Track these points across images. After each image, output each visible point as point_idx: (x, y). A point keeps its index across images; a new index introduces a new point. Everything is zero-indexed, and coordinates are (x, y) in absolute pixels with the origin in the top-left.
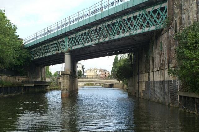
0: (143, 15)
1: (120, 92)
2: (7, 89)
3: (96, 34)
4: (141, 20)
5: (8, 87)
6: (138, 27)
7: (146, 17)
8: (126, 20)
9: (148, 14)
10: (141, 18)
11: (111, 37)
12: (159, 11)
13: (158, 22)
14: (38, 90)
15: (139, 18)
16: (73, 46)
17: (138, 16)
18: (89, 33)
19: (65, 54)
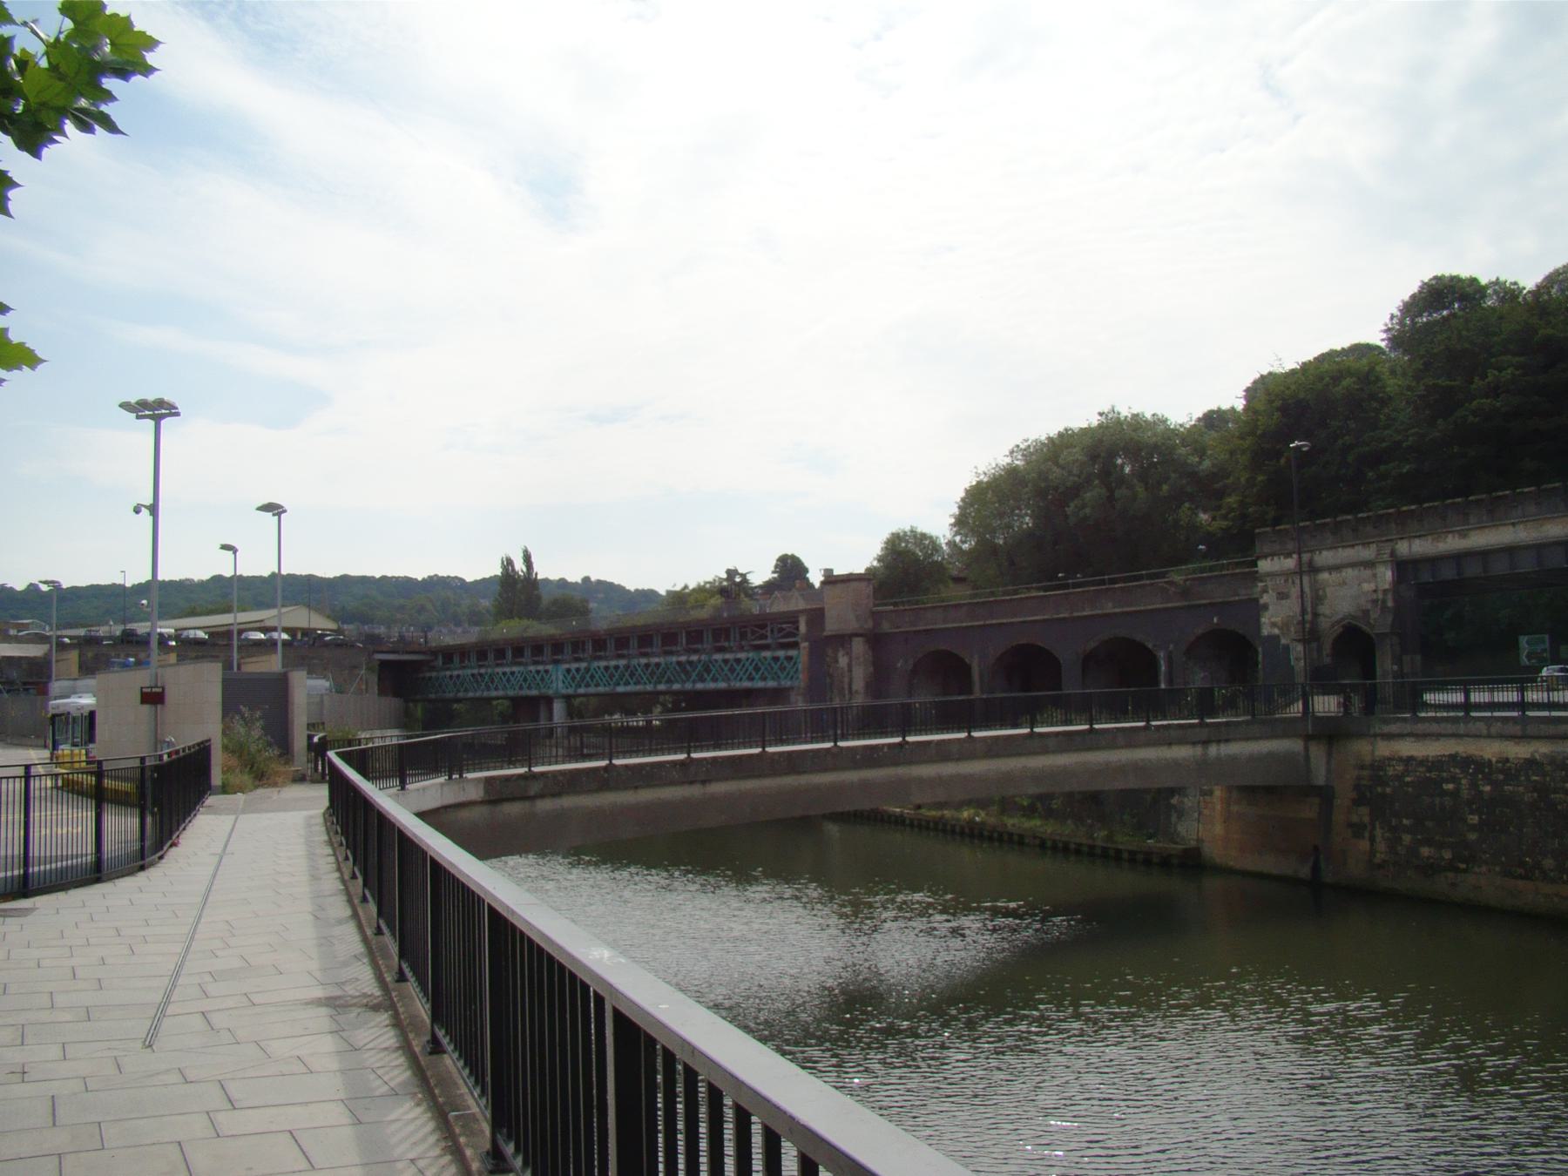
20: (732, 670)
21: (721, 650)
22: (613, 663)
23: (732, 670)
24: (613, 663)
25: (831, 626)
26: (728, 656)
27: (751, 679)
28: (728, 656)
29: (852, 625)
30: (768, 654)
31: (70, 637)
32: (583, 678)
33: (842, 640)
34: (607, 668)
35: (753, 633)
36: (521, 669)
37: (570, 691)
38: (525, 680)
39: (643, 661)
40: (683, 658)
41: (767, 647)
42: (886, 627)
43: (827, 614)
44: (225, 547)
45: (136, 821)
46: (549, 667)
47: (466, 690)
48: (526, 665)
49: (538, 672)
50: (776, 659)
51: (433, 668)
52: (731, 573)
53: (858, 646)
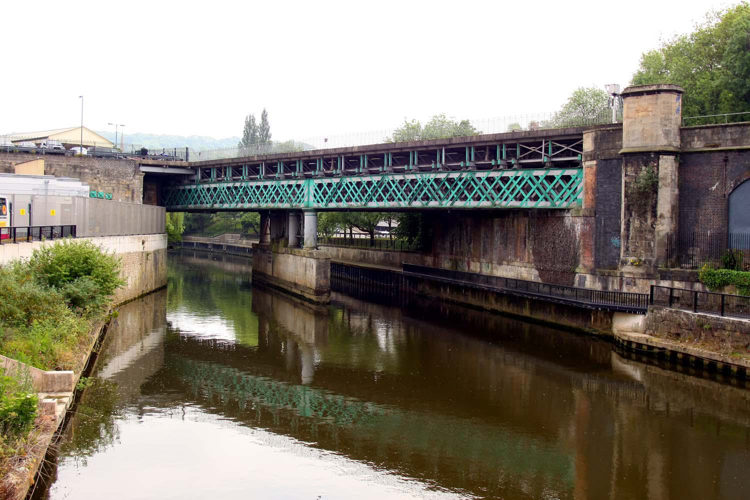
0: (275, 187)
1: (108, 253)
2: (747, 313)
3: (402, 190)
4: (273, 193)
5: (359, 269)
6: (269, 200)
7: (474, 186)
8: (261, 188)
9: (281, 187)
10: (274, 190)
11: (232, 205)
12: (558, 181)
13: (294, 200)
14: (662, 312)
15: (271, 189)
16: (173, 204)
17: (512, 179)
18: (339, 186)
19: (306, 214)
20: (262, 194)
23: (262, 194)
24: (365, 179)
30: (541, 173)
37: (322, 205)
39: (398, 177)
40: (231, 185)
51: (193, 182)
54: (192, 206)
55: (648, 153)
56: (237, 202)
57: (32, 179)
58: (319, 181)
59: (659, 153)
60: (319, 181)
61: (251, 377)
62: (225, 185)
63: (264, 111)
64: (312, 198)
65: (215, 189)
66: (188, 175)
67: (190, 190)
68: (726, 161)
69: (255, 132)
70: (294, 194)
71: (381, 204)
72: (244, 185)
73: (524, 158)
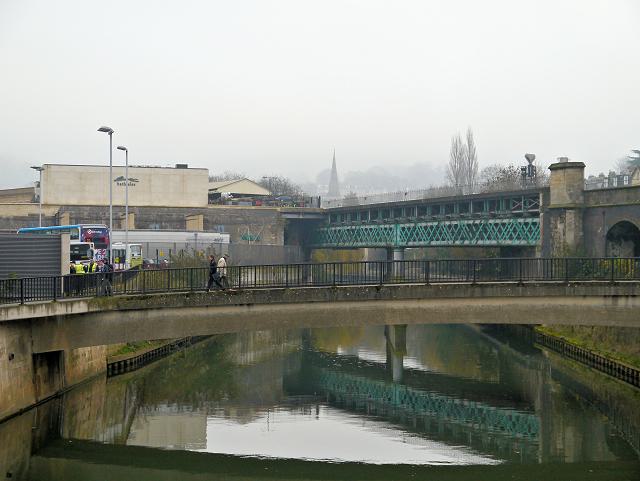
20: (500, 231)
21: (494, 217)
22: (430, 224)
23: (500, 231)
24: (430, 224)
25: (554, 202)
26: (498, 221)
27: (511, 238)
28: (498, 221)
29: (567, 201)
30: (521, 220)
31: (500, 354)
32: (435, 234)
33: (560, 211)
34: (426, 228)
35: (514, 204)
36: (376, 227)
37: (404, 244)
38: (515, 231)
39: (447, 223)
40: (471, 222)
41: (519, 216)
42: (592, 203)
43: (552, 192)
44: (102, 130)
45: (404, 365)
46: (392, 226)
47: (344, 241)
48: (379, 224)
49: (386, 229)
50: (526, 224)
51: (324, 225)
52: (351, 193)
53: (570, 216)
54: (325, 245)
55: (560, 208)
56: (477, 239)
57: (20, 417)
58: (402, 226)
59: (565, 209)
60: (402, 226)
61: (493, 408)
62: (346, 228)
63: (469, 131)
64: (399, 239)
65: (339, 231)
66: (323, 220)
67: (323, 232)
68: (604, 213)
69: (463, 159)
70: (530, 231)
71: (438, 243)
72: (358, 227)
73: (532, 208)
